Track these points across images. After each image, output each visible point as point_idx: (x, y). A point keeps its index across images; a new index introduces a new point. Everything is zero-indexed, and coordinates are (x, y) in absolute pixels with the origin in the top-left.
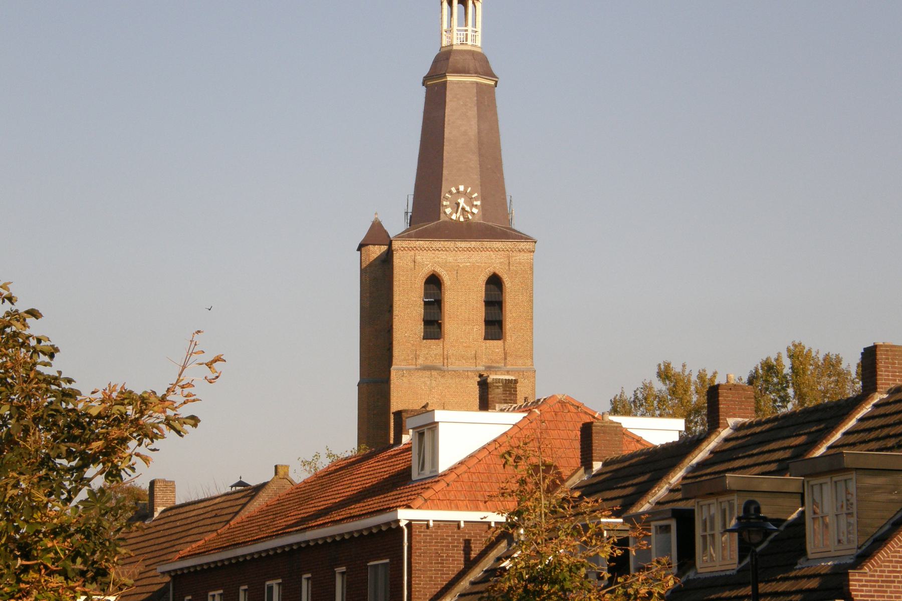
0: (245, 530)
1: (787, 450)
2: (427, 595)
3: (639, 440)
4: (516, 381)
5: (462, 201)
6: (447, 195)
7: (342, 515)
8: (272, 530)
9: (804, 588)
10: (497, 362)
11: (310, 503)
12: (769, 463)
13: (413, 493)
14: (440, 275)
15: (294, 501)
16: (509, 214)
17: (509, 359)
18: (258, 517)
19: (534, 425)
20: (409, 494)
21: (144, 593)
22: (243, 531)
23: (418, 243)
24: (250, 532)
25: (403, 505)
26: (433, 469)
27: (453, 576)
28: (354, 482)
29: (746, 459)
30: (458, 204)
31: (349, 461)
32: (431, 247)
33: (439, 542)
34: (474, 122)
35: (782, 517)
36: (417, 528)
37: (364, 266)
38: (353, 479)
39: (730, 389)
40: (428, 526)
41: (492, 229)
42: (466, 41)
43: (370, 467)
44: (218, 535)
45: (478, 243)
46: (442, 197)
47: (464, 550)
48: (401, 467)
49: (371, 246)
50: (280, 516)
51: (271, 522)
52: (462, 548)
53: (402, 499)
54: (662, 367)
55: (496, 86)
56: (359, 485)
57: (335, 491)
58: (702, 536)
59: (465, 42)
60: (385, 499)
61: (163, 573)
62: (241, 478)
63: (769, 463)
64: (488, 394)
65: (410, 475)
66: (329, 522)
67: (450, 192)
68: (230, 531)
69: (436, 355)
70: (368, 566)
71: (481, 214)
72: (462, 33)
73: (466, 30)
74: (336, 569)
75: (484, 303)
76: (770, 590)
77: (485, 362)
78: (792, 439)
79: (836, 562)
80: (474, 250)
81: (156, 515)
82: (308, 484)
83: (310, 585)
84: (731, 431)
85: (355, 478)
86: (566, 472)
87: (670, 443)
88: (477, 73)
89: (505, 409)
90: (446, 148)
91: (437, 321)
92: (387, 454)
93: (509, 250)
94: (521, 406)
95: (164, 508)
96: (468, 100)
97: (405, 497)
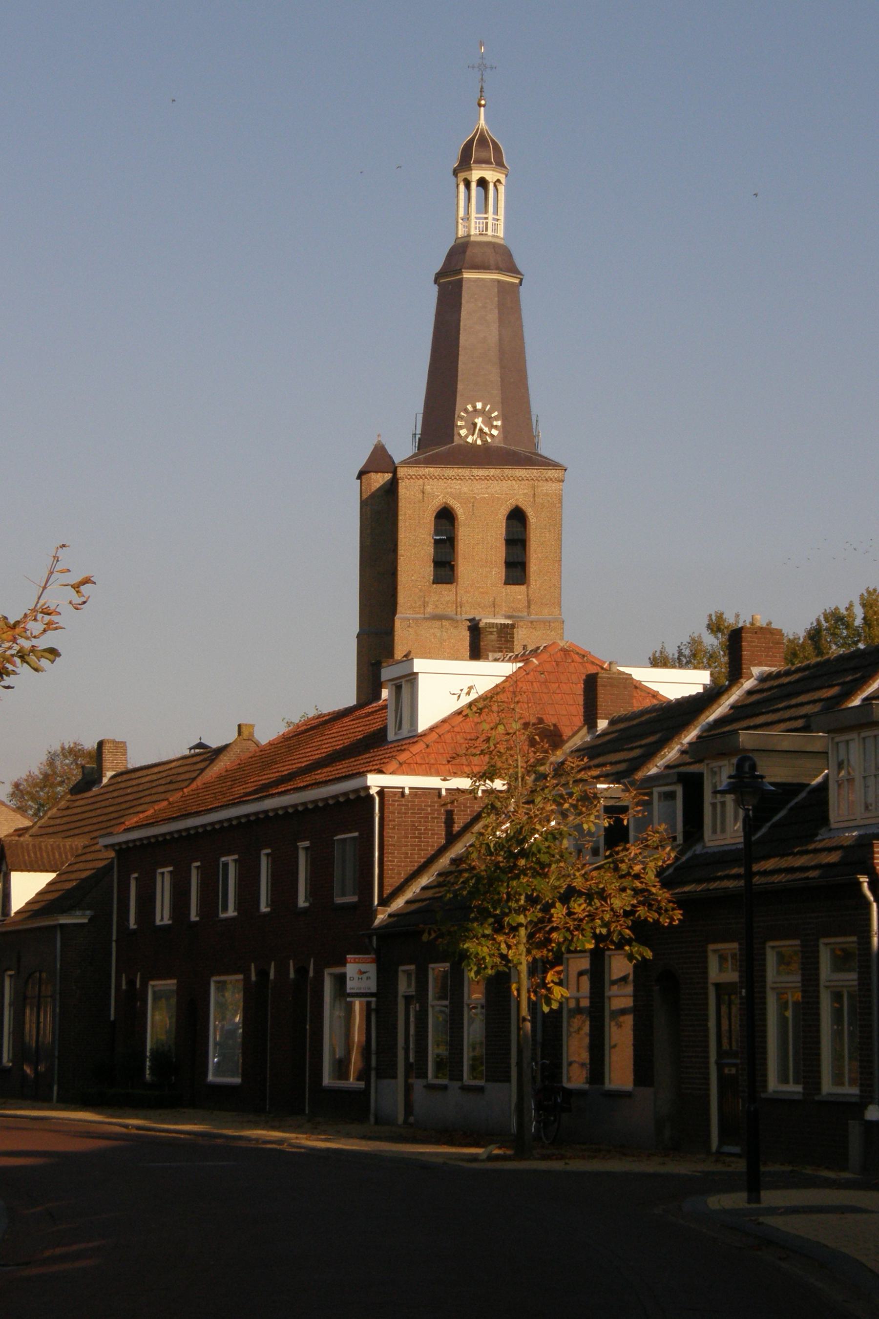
0: (199, 799)
1: (817, 704)
2: (401, 874)
3: (655, 695)
4: (513, 626)
5: (479, 421)
6: (462, 414)
7: (306, 781)
8: (229, 798)
9: (824, 862)
10: (519, 611)
11: (274, 767)
12: (796, 718)
13: (387, 756)
14: (452, 509)
15: (256, 765)
16: (535, 437)
17: (533, 607)
18: (215, 783)
19: (530, 677)
20: (382, 757)
21: (87, 870)
22: (197, 799)
23: (427, 470)
24: (204, 801)
25: (375, 770)
26: (413, 728)
27: (433, 852)
28: (324, 744)
29: (770, 714)
30: (475, 425)
31: (321, 720)
32: (443, 475)
33: (415, 813)
34: (494, 328)
35: (804, 781)
36: (391, 797)
37: (364, 497)
38: (323, 740)
39: (756, 633)
40: (403, 794)
41: (515, 454)
42: (487, 230)
43: (344, 727)
44: (170, 804)
45: (499, 471)
46: (456, 416)
47: (445, 823)
48: (377, 726)
49: (372, 474)
50: (239, 782)
51: (228, 789)
52: (443, 820)
53: (374, 763)
54: (714, 618)
55: (521, 285)
56: (329, 747)
57: (301, 754)
58: (711, 803)
59: (484, 232)
60: (355, 763)
61: (106, 847)
62: (200, 739)
63: (796, 718)
64: (480, 641)
65: (386, 735)
66: (291, 790)
67: (466, 410)
68: (183, 799)
69: (448, 602)
70: (334, 840)
71: (502, 436)
72: (481, 221)
73: (486, 218)
74: (298, 844)
75: (504, 542)
76: (785, 866)
77: (505, 611)
78: (825, 690)
79: (862, 832)
80: (493, 478)
81: (105, 780)
82: (273, 746)
83: (270, 862)
84: (756, 682)
85: (326, 739)
86: (566, 732)
87: (686, 697)
88: (499, 269)
89: (499, 659)
90: (461, 358)
91: (449, 563)
92: (364, 712)
93: (535, 479)
94: (517, 655)
95: (114, 773)
96: (488, 301)
97: (378, 760)
